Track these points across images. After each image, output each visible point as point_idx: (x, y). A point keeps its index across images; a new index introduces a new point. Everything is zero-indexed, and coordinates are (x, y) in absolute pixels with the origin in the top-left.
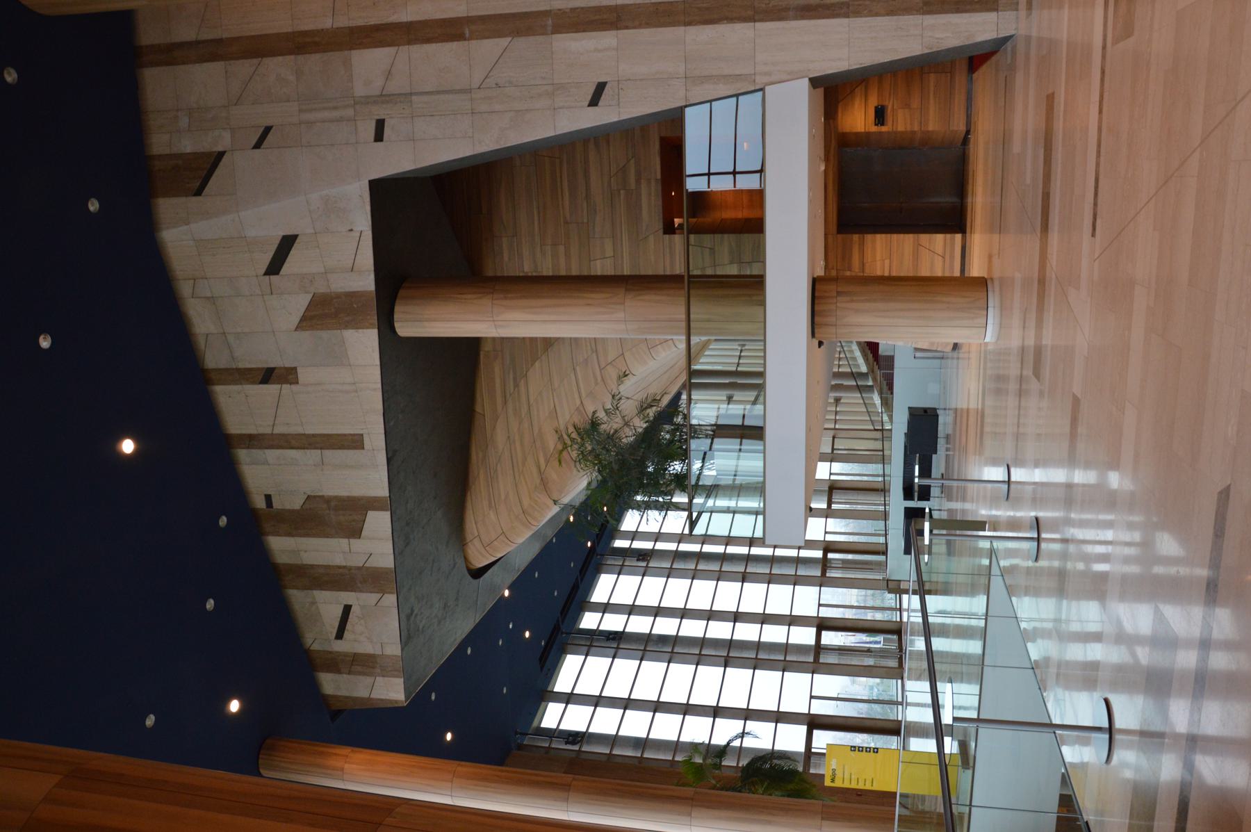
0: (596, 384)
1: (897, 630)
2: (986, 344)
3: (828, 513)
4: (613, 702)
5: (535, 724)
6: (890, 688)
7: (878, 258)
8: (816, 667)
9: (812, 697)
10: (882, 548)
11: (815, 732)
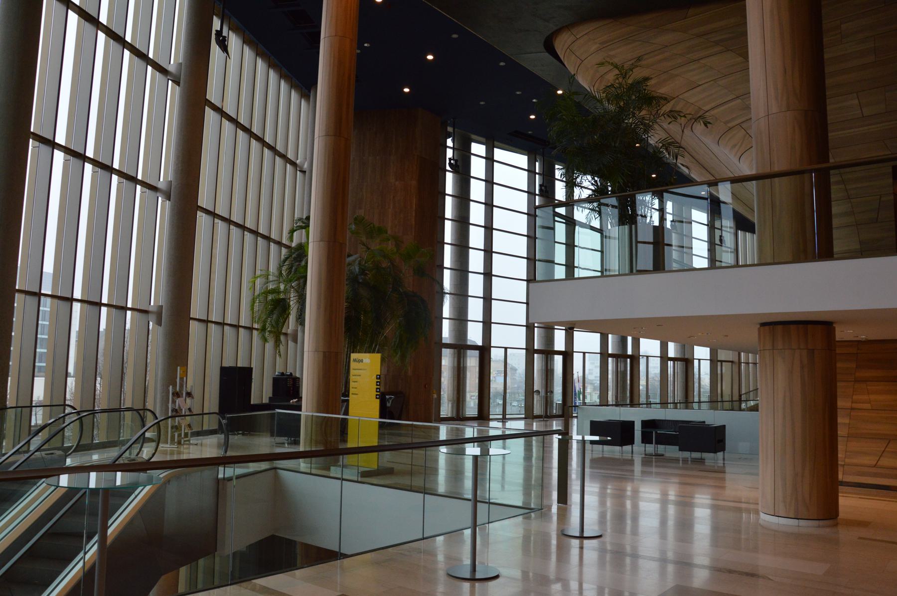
0: (726, 123)
1: (483, 416)
2: (757, 512)
3: (664, 358)
4: (489, 194)
5: (474, 137)
6: (516, 405)
7: (872, 397)
8: (530, 351)
9: (506, 349)
10: (636, 402)
11: (477, 352)
